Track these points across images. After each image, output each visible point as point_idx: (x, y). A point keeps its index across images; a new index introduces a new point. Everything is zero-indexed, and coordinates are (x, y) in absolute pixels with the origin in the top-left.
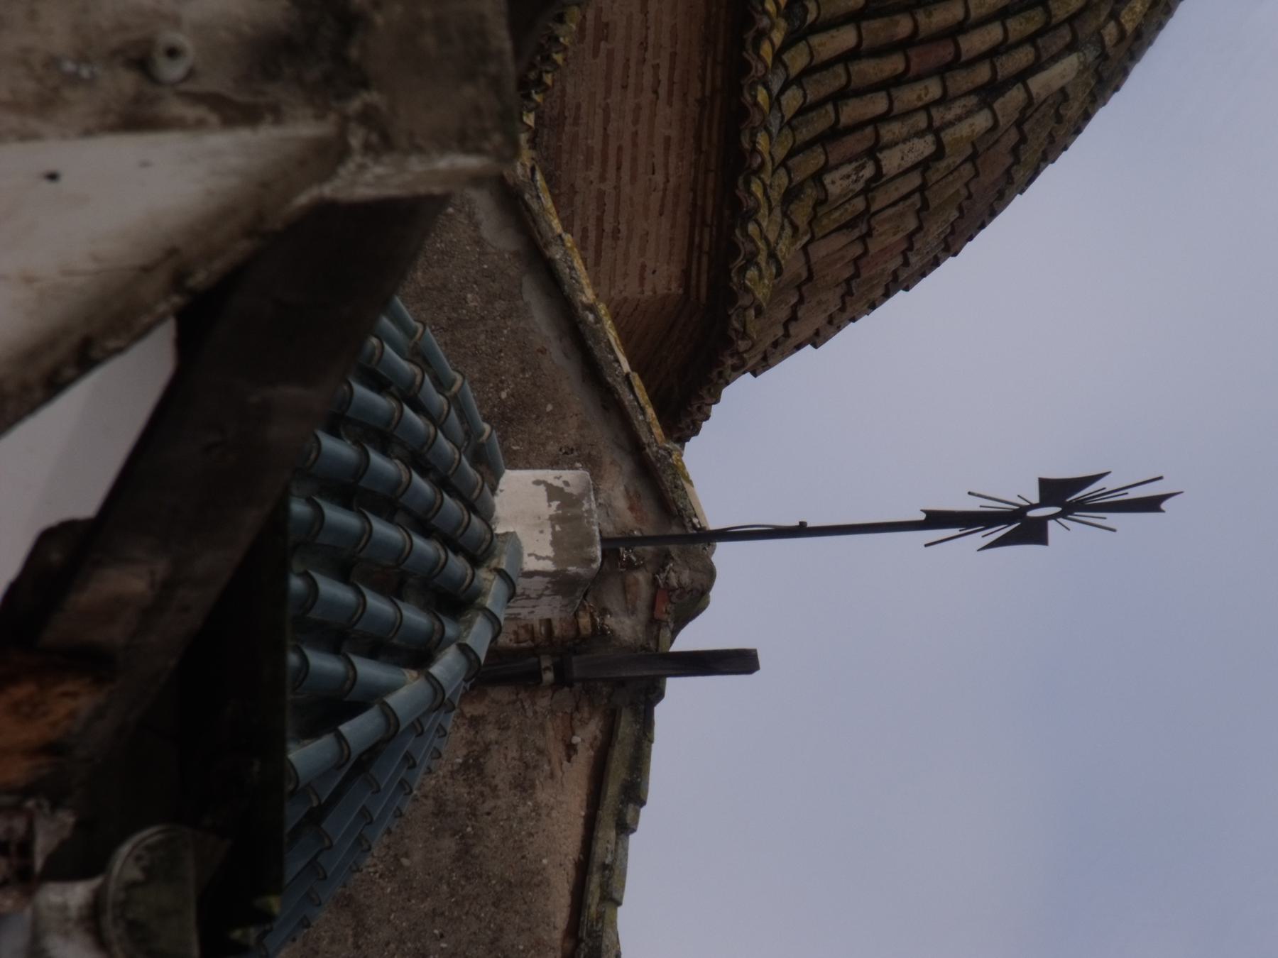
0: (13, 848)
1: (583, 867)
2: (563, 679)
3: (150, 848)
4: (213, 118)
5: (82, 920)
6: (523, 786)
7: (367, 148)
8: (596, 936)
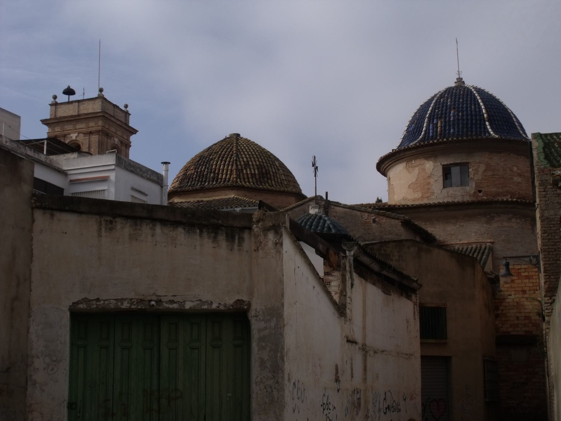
2: (328, 209)
4: (282, 238)
6: (336, 212)
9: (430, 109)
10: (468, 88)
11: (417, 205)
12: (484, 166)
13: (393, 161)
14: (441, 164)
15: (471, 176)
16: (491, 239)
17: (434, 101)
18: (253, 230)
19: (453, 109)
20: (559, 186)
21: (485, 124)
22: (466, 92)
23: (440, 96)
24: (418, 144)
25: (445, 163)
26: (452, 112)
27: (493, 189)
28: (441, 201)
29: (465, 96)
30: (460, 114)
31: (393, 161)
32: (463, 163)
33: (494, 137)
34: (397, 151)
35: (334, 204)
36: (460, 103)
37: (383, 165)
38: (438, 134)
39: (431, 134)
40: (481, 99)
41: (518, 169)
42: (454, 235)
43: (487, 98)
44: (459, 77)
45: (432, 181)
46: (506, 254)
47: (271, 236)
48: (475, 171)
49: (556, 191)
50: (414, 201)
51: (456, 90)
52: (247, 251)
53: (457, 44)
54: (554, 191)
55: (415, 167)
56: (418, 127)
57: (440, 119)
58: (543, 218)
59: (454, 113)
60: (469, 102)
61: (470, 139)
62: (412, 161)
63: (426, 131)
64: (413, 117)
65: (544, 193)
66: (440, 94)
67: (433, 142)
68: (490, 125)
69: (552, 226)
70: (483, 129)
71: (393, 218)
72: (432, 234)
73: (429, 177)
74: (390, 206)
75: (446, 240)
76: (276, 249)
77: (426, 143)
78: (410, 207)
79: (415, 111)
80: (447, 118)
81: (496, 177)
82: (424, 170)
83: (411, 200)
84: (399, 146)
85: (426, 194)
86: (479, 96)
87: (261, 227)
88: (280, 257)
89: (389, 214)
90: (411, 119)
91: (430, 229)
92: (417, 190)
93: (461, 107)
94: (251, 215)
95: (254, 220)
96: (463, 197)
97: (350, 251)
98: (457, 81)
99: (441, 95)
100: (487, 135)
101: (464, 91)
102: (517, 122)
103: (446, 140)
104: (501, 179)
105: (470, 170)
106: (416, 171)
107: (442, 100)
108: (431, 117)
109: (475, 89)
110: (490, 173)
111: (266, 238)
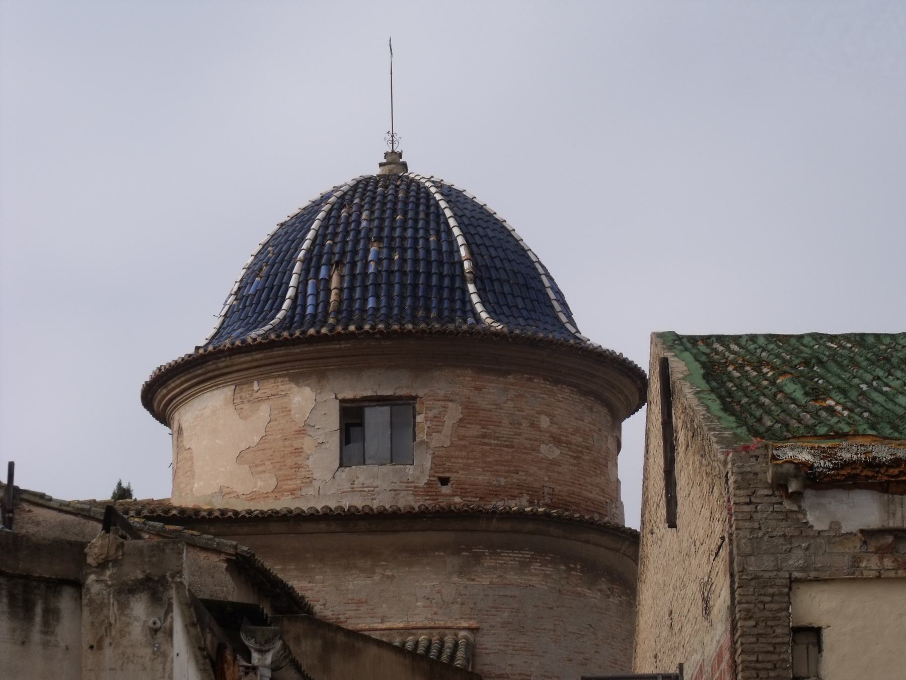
0: (247, 671)
1: (60, 511)
2: (12, 511)
3: (246, 637)
4: (171, 614)
5: (262, 655)
6: (38, 524)
7: (180, 577)
8: (78, 509)
9: (310, 235)
10: (418, 184)
11: (262, 512)
12: (460, 408)
13: (195, 381)
14: (336, 398)
15: (421, 436)
16: (471, 619)
17: (321, 215)
18: (88, 590)
19: (374, 241)
20: (790, 490)
21: (465, 291)
22: (412, 193)
23: (340, 201)
24: (273, 336)
25: (349, 395)
26: (373, 249)
27: (480, 478)
28: (333, 505)
29: (411, 206)
30: (396, 257)
31: (195, 381)
32: (400, 398)
33: (492, 329)
34: (210, 352)
35: (32, 499)
36: (398, 224)
37: (165, 391)
38: (331, 309)
39: (310, 310)
40: (455, 216)
41: (552, 422)
42: (366, 602)
43: (473, 217)
44: (393, 151)
45: (307, 443)
46: (511, 665)
47: (139, 608)
48: (431, 421)
49: (781, 503)
50: (252, 499)
51: (386, 187)
52: (67, 648)
53: (391, 56)
54: (775, 504)
55: (260, 400)
56: (273, 286)
57: (337, 267)
58: (744, 577)
59: (378, 253)
60: (421, 224)
61: (423, 331)
62: (253, 382)
63: (294, 300)
64: (256, 256)
65: (747, 508)
66: (338, 194)
67: (318, 332)
68: (480, 292)
69: (768, 599)
70: (458, 305)
71: (205, 549)
72: (303, 598)
73: (301, 432)
74: (182, 511)
75: (342, 618)
76: (154, 646)
77: (297, 333)
78: (244, 516)
79: (264, 239)
80: (359, 264)
81: (492, 442)
82: (286, 411)
83: (244, 497)
84: (213, 337)
85: (289, 482)
86: (451, 209)
87: (109, 583)
88: (164, 669)
89: (192, 535)
90: (252, 262)
91: (299, 584)
92: (263, 468)
93: (387, 236)
94: (83, 545)
95: (90, 560)
96: (396, 494)
97: (262, 652)
98: (385, 161)
99: (342, 197)
100: (470, 320)
101: (407, 191)
102: (552, 288)
103: (357, 328)
104: (505, 449)
105: (419, 419)
106: (262, 414)
107: (344, 213)
108: (311, 259)
109: (437, 187)
110: (475, 430)
111: (126, 613)
